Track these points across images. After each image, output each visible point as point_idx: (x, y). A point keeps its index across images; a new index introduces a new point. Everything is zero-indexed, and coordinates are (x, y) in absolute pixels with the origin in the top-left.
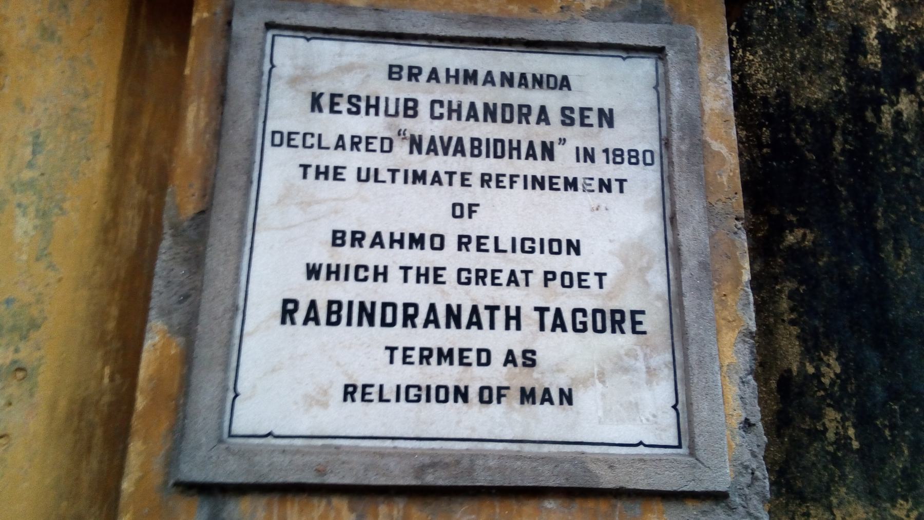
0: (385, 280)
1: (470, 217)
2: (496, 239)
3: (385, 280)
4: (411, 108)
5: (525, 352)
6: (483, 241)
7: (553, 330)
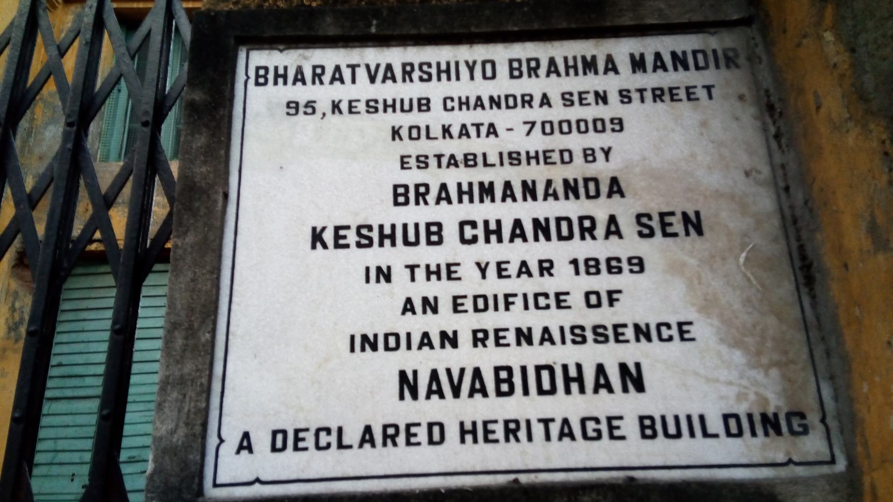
0: (462, 424)
3: (462, 424)
4: (434, 233)
5: (630, 101)
6: (501, 334)
7: (596, 391)
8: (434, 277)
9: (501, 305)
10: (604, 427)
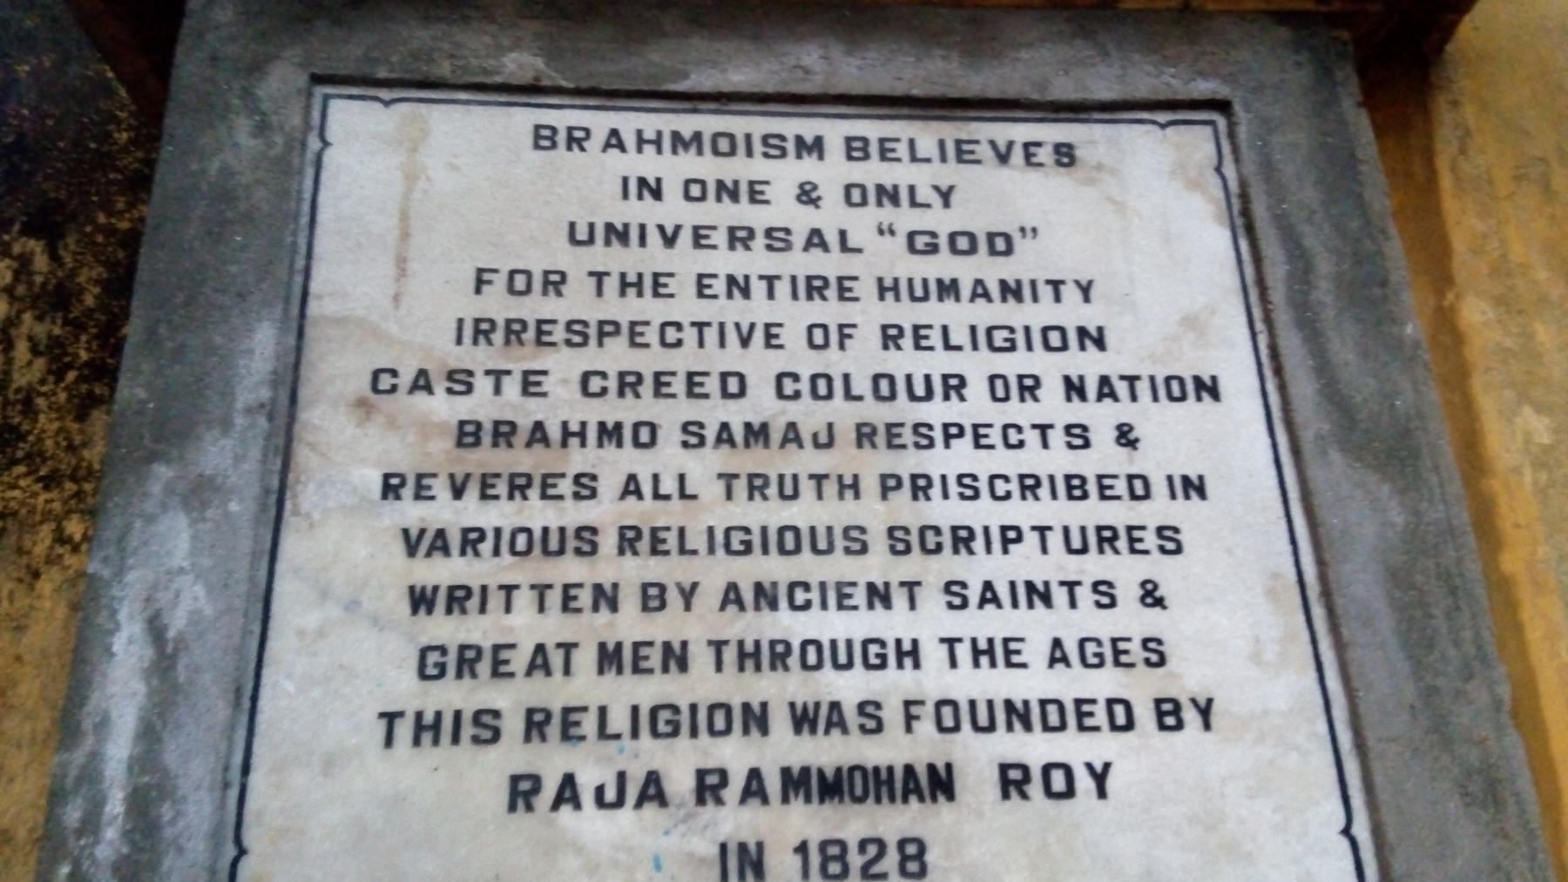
1: (842, 346)
2: (945, 329)
6: (546, 327)
8: (632, 291)
9: (997, 545)
10: (1107, 651)
